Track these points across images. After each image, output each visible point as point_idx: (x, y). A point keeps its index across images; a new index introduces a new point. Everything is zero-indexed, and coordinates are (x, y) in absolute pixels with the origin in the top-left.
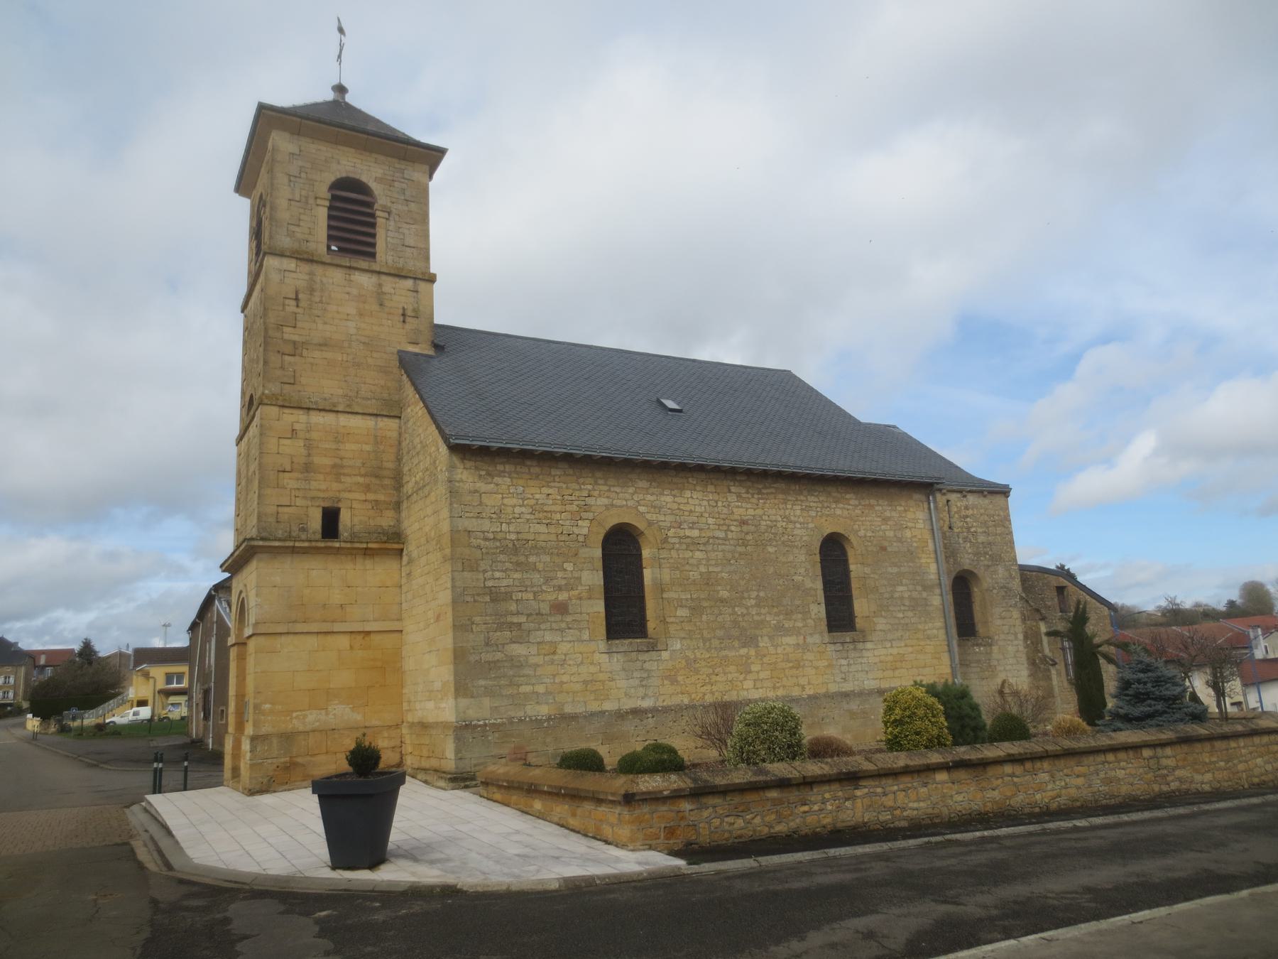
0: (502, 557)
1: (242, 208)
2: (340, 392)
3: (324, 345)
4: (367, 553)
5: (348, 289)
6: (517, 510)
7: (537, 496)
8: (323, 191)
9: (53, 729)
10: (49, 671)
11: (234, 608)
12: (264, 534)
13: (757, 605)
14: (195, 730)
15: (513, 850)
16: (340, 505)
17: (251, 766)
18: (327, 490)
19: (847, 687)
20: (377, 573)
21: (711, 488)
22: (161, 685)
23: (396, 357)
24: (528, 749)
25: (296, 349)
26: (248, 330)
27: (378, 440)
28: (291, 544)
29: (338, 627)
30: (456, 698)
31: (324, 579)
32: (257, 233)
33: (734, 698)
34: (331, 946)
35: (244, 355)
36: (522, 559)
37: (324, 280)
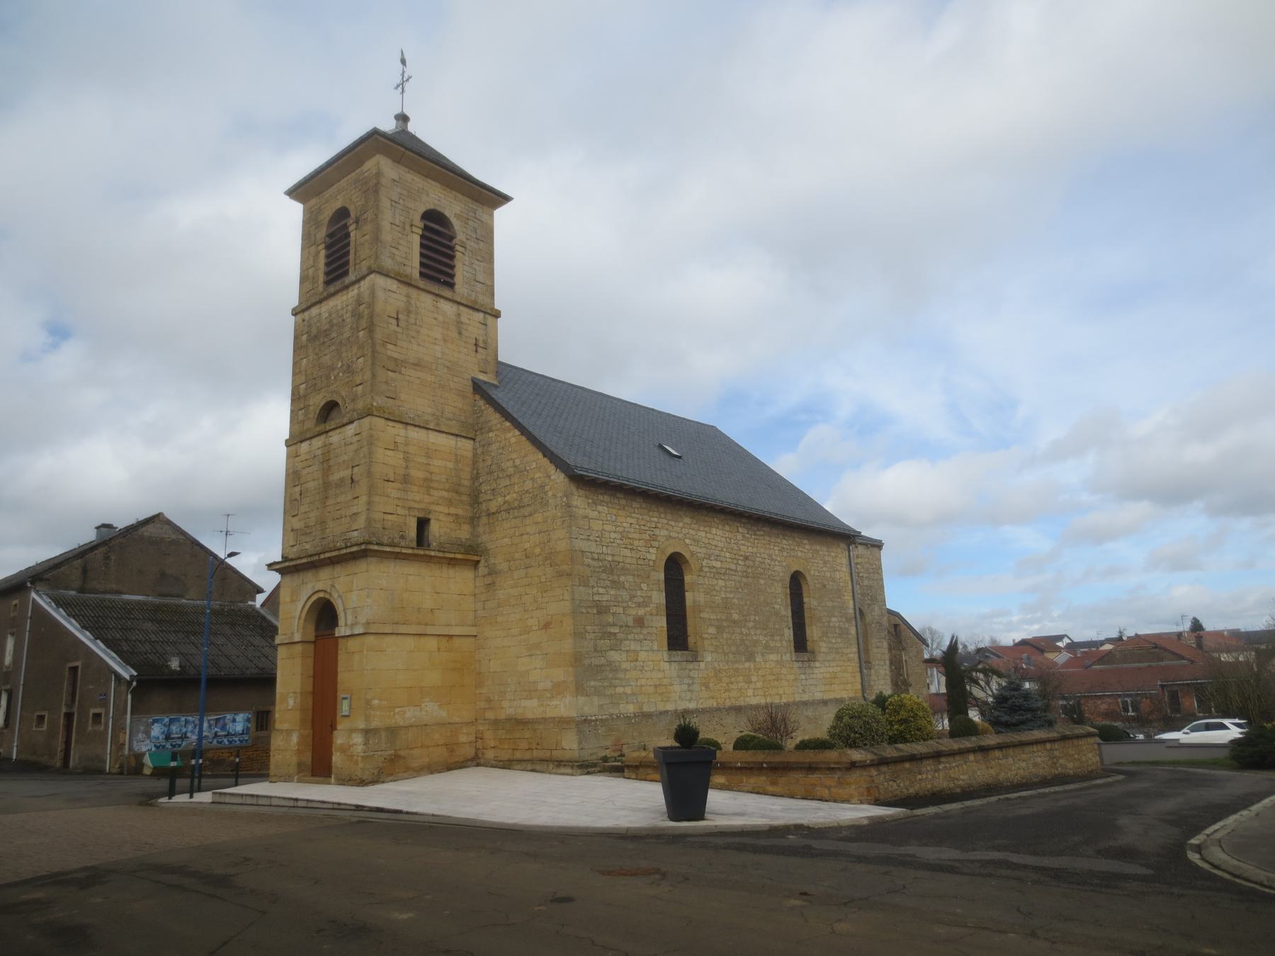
3: (418, 365)
4: (452, 562)
6: (613, 535)
13: (755, 628)
18: (419, 502)
19: (806, 697)
20: (459, 581)
21: (727, 528)
24: (624, 741)
25: (397, 366)
27: (458, 459)
29: (430, 630)
33: (742, 703)
36: (616, 578)
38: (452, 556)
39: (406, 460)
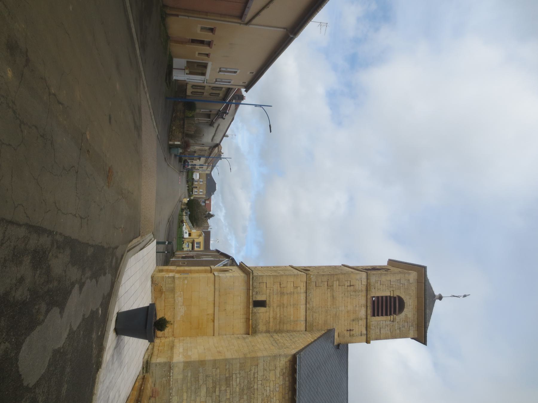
0: (246, 382)
1: (384, 263)
2: (314, 305)
4: (248, 320)
5: (358, 306)
6: (268, 388)
7: (275, 398)
8: (397, 294)
9: (183, 207)
10: (203, 204)
11: (225, 267)
12: (255, 278)
14: (179, 254)
15: (111, 395)
16: (267, 307)
17: (163, 277)
20: (239, 323)
22: (196, 241)
23: (332, 328)
24: (157, 398)
25: (330, 286)
26: (335, 267)
28: (251, 288)
30: (183, 362)
31: (237, 303)
32: (374, 269)
34: (86, 317)
35: (325, 267)
36: (245, 392)
37: (360, 296)
38: (251, 318)
39: (291, 293)
